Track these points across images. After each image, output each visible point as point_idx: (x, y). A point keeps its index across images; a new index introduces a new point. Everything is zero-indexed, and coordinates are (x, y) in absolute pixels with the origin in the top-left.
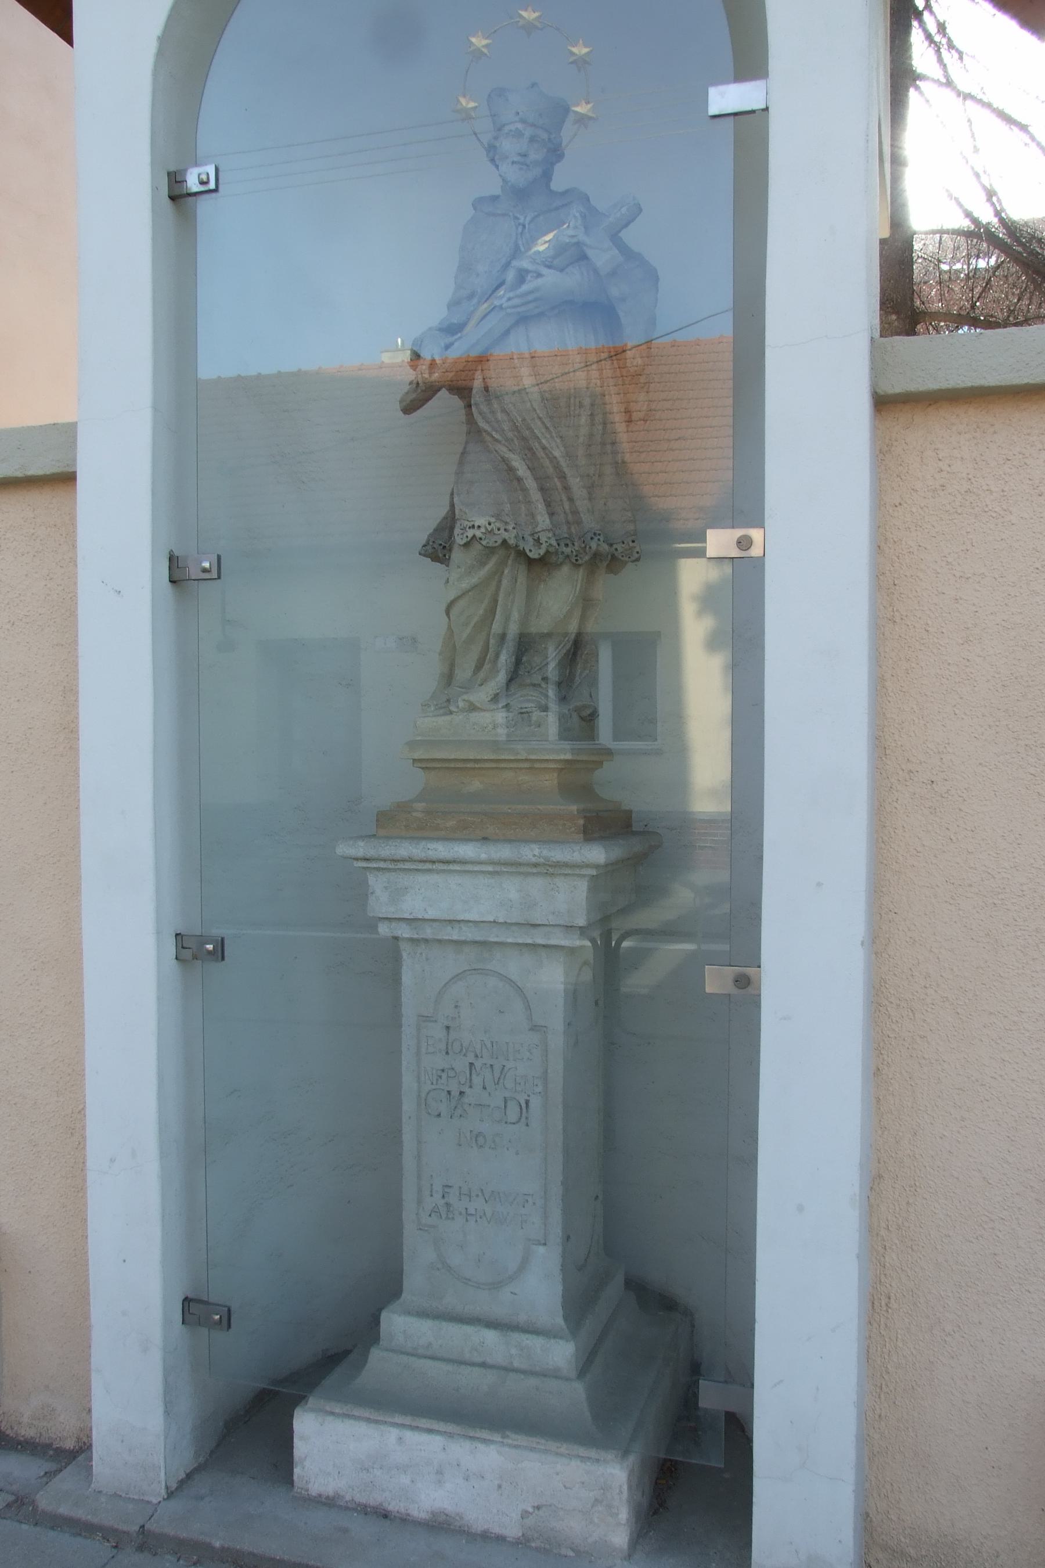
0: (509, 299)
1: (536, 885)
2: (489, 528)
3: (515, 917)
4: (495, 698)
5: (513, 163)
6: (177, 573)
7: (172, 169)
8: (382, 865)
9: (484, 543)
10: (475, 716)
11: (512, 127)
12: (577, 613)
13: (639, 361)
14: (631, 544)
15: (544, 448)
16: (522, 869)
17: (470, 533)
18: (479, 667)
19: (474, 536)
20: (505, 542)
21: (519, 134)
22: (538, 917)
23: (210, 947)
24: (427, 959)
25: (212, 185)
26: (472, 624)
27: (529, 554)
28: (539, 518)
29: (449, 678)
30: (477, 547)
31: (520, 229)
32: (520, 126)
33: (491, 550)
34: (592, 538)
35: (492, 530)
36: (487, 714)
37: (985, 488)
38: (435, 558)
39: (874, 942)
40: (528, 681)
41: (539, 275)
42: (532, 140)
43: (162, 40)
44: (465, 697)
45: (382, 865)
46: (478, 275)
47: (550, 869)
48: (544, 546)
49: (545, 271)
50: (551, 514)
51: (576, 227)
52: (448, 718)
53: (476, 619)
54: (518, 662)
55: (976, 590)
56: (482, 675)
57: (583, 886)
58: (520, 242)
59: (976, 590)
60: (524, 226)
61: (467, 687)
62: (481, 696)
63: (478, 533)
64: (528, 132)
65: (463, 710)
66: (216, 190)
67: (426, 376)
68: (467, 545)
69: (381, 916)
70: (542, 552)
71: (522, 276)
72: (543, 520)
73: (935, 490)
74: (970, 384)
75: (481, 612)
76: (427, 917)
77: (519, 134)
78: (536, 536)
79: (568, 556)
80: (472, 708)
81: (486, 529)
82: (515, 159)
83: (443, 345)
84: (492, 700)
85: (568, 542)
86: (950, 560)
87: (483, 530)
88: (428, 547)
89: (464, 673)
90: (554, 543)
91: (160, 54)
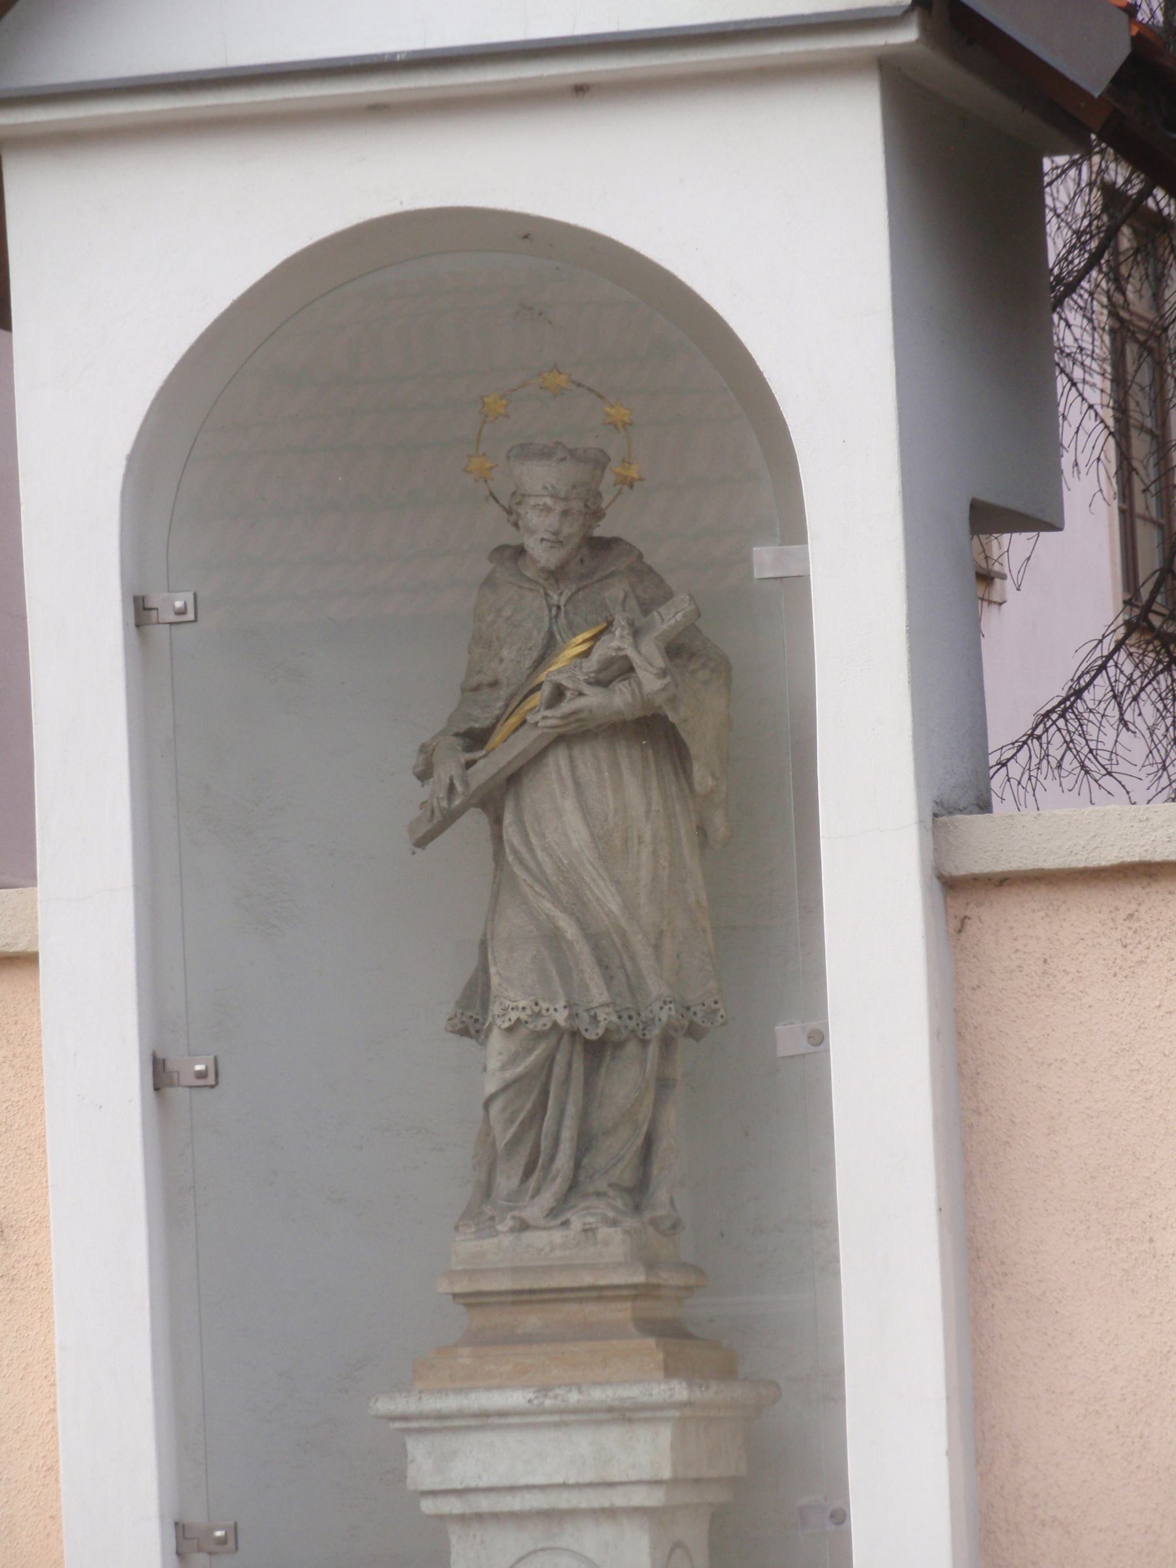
0: (544, 718)
1: (612, 1436)
2: (536, 1009)
3: (589, 1476)
4: (553, 1213)
5: (542, 540)
6: (160, 1075)
7: (139, 594)
8: (425, 1424)
9: (531, 1026)
10: (528, 1237)
11: (541, 501)
12: (649, 1099)
13: (710, 782)
14: (713, 1006)
15: (598, 900)
16: (594, 1416)
17: (514, 1016)
18: (528, 1173)
19: (518, 1020)
20: (555, 1025)
21: (547, 509)
22: (614, 1474)
23: (219, 1534)
24: (483, 1542)
25: (190, 616)
26: (518, 1122)
27: (584, 1033)
28: (594, 990)
29: (487, 1190)
30: (523, 1031)
31: (554, 611)
32: (549, 501)
33: (539, 1036)
34: (661, 1008)
35: (540, 1012)
36: (544, 1234)
37: (1061, 968)
38: (464, 1032)
39: (977, 1461)
40: (591, 1189)
41: (581, 694)
42: (565, 513)
43: (131, 458)
44: (516, 1213)
45: (425, 1424)
46: (501, 660)
47: (623, 1415)
48: (603, 1024)
49: (586, 689)
50: (609, 980)
51: (622, 637)
52: (495, 1240)
53: (522, 1116)
54: (578, 1165)
55: (1059, 1077)
56: (532, 1183)
57: (665, 1435)
58: (555, 628)
59: (1059, 1077)
60: (559, 608)
61: (515, 1197)
62: (533, 1211)
63: (524, 1016)
64: (559, 507)
65: (512, 1230)
66: (196, 620)
67: (444, 804)
68: (510, 1030)
69: (424, 1488)
70: (601, 1032)
71: (559, 693)
72: (598, 993)
73: (1012, 972)
74: (1031, 867)
75: (529, 1106)
76: (482, 1484)
77: (547, 509)
78: (592, 1012)
79: (633, 1031)
80: (523, 1226)
81: (533, 1011)
82: (545, 537)
83: (463, 761)
84: (547, 1216)
85: (632, 1013)
86: (1031, 1045)
87: (528, 1012)
88: (456, 1021)
89: (506, 1182)
90: (614, 1018)
91: (129, 469)
